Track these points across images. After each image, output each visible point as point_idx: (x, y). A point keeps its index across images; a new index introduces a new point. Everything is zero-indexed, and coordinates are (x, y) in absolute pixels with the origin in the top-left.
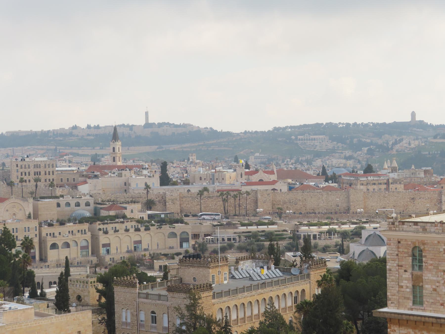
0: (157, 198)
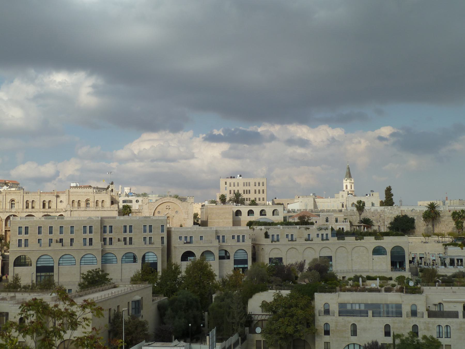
0: (373, 217)
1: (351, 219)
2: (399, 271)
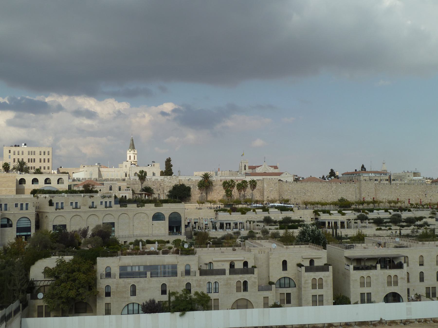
0: (154, 185)
2: (176, 234)
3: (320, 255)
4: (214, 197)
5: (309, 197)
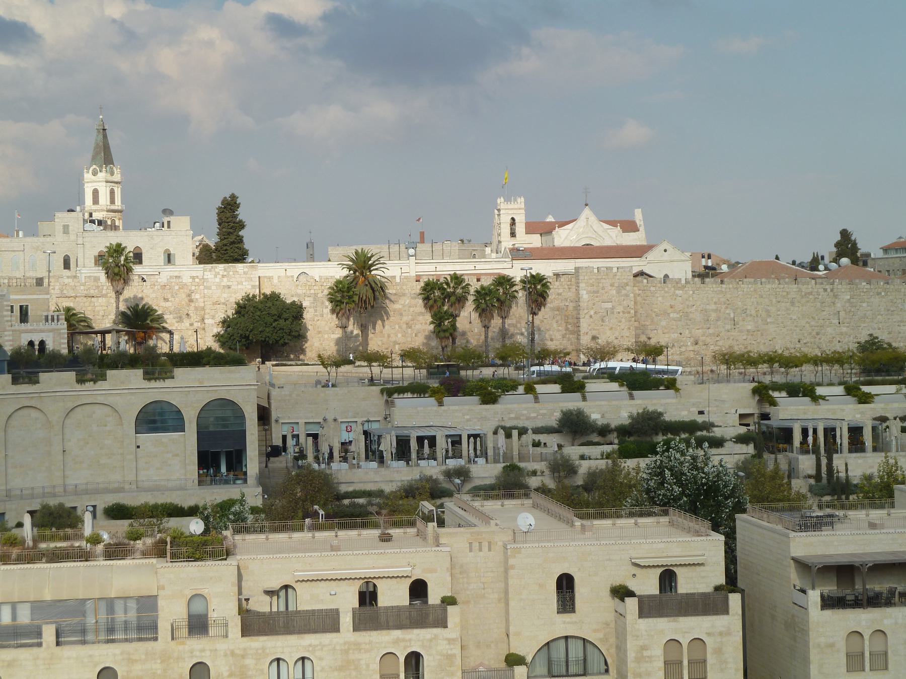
0: (166, 300)
1: (90, 308)
2: (227, 482)
3: (700, 553)
4: (393, 339)
5: (749, 337)
